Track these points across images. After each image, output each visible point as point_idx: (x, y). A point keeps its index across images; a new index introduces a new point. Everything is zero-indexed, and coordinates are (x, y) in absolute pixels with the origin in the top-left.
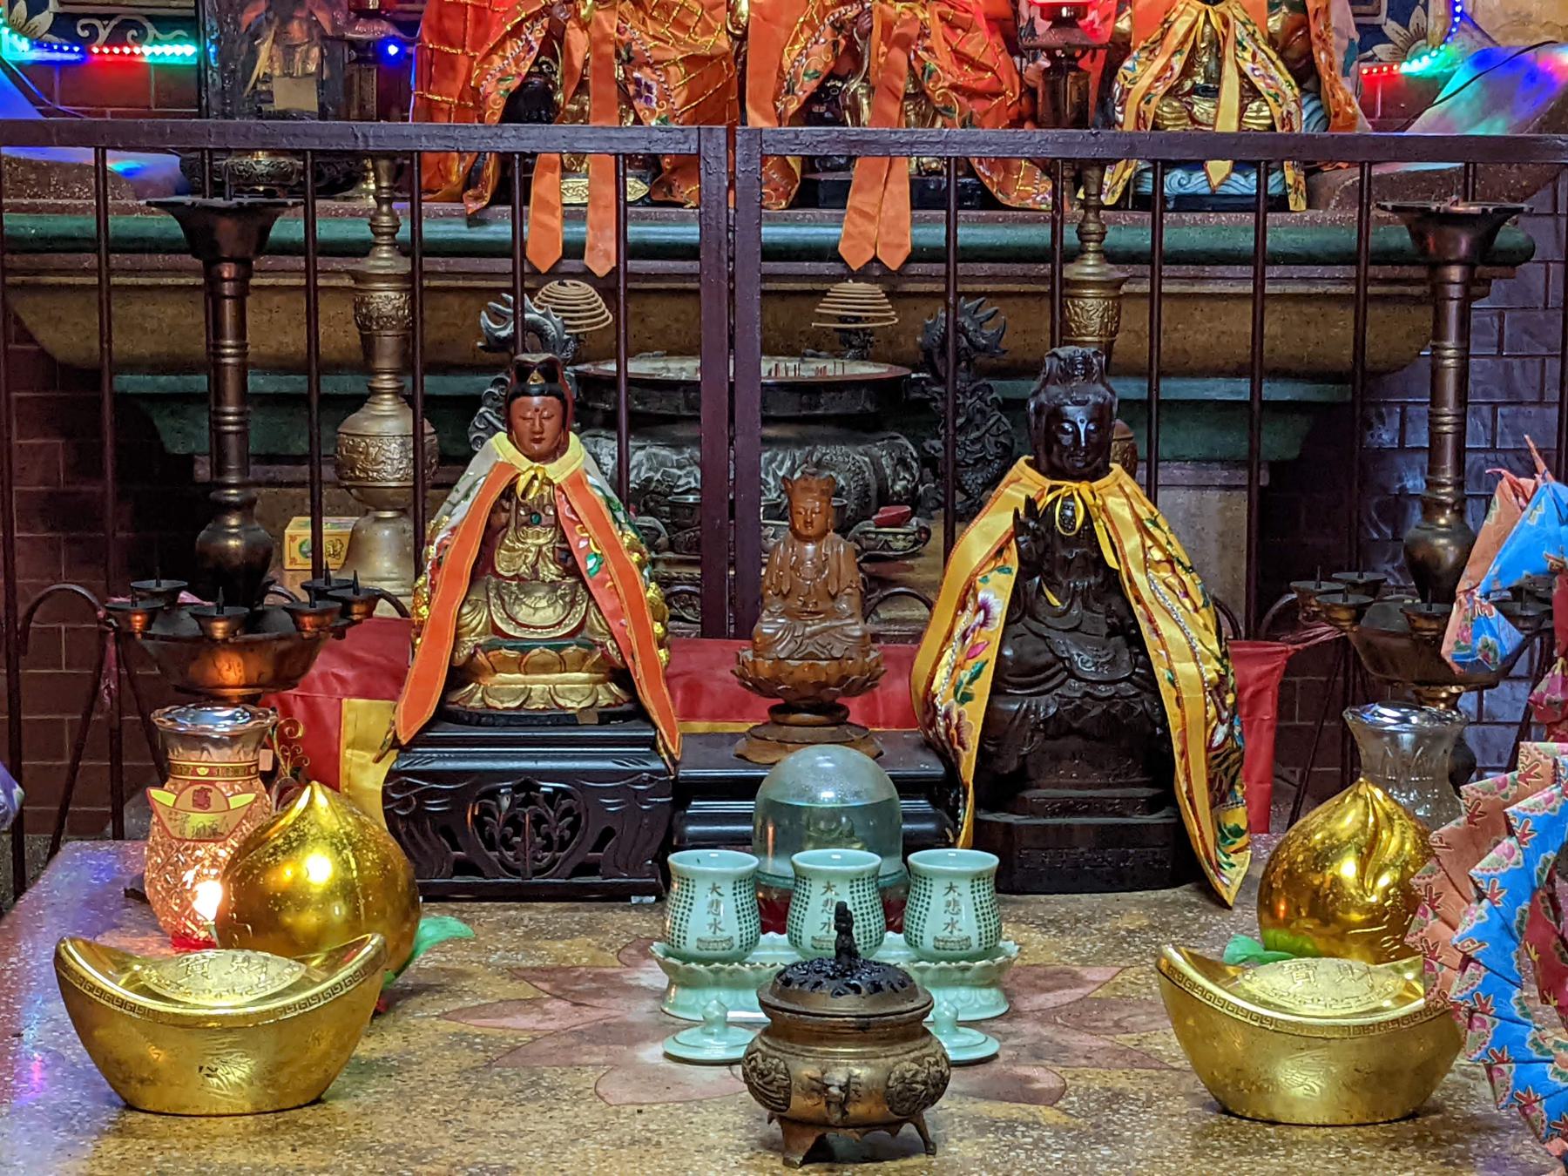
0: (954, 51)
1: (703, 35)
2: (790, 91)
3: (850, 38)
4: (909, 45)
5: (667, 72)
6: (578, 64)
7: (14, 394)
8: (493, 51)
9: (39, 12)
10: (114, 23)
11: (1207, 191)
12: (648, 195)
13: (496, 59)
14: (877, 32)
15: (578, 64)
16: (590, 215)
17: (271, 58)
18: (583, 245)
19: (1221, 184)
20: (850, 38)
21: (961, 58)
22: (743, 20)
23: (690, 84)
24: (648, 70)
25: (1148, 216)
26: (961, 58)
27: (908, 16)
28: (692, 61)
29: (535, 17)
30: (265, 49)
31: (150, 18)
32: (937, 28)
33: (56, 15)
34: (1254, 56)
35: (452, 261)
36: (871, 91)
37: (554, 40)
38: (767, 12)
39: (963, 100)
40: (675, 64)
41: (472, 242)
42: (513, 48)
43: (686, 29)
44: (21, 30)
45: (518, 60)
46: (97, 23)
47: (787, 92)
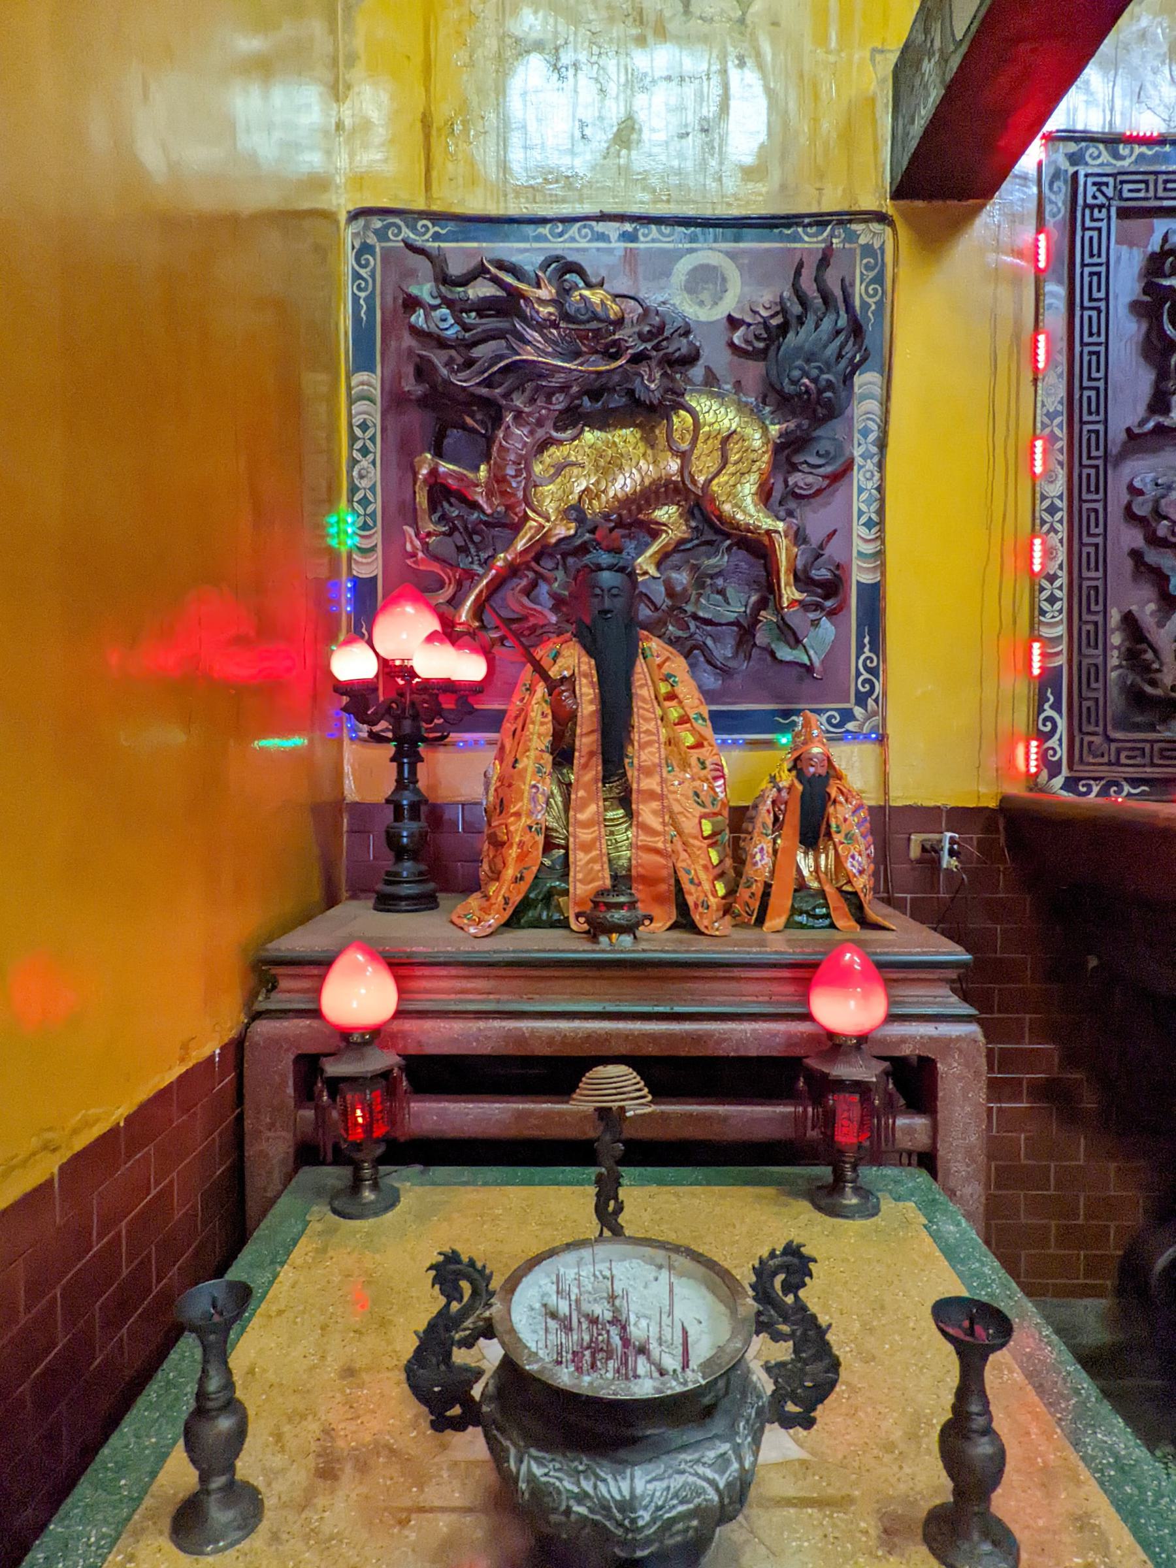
7: (993, 1222)
9: (1055, 776)
10: (1103, 782)
31: (1126, 779)
33: (1067, 778)
46: (1092, 782)
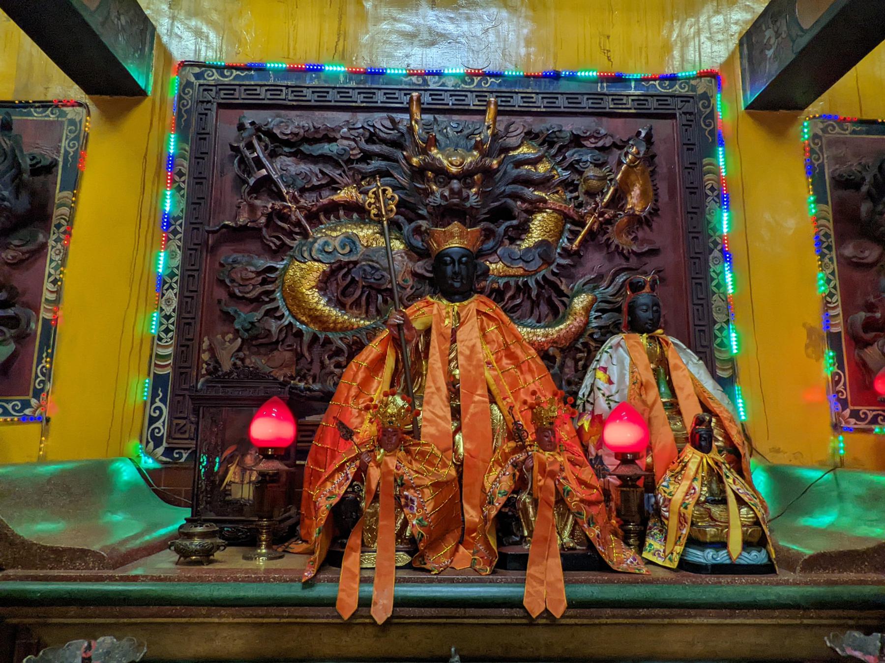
0: (577, 478)
1: (442, 468)
2: (491, 503)
3: (521, 471)
4: (555, 476)
5: (423, 492)
6: (374, 487)
8: (327, 480)
9: (158, 447)
11: (728, 562)
12: (410, 563)
13: (328, 484)
14: (536, 468)
15: (374, 487)
16: (376, 580)
17: (234, 473)
18: (371, 599)
19: (738, 558)
20: (521, 471)
21: (581, 482)
22: (461, 457)
23: (435, 498)
24: (412, 491)
25: (674, 565)
26: (581, 482)
27: (551, 459)
28: (436, 485)
29: (352, 460)
30: (232, 469)
32: (567, 465)
34: (734, 481)
35: (293, 609)
36: (535, 503)
37: (361, 474)
38: (472, 454)
39: (587, 507)
40: (427, 487)
41: (304, 599)
42: (339, 478)
43: (433, 465)
44: (150, 454)
45: (340, 485)
47: (489, 503)
